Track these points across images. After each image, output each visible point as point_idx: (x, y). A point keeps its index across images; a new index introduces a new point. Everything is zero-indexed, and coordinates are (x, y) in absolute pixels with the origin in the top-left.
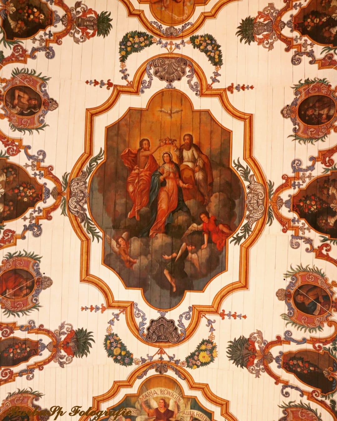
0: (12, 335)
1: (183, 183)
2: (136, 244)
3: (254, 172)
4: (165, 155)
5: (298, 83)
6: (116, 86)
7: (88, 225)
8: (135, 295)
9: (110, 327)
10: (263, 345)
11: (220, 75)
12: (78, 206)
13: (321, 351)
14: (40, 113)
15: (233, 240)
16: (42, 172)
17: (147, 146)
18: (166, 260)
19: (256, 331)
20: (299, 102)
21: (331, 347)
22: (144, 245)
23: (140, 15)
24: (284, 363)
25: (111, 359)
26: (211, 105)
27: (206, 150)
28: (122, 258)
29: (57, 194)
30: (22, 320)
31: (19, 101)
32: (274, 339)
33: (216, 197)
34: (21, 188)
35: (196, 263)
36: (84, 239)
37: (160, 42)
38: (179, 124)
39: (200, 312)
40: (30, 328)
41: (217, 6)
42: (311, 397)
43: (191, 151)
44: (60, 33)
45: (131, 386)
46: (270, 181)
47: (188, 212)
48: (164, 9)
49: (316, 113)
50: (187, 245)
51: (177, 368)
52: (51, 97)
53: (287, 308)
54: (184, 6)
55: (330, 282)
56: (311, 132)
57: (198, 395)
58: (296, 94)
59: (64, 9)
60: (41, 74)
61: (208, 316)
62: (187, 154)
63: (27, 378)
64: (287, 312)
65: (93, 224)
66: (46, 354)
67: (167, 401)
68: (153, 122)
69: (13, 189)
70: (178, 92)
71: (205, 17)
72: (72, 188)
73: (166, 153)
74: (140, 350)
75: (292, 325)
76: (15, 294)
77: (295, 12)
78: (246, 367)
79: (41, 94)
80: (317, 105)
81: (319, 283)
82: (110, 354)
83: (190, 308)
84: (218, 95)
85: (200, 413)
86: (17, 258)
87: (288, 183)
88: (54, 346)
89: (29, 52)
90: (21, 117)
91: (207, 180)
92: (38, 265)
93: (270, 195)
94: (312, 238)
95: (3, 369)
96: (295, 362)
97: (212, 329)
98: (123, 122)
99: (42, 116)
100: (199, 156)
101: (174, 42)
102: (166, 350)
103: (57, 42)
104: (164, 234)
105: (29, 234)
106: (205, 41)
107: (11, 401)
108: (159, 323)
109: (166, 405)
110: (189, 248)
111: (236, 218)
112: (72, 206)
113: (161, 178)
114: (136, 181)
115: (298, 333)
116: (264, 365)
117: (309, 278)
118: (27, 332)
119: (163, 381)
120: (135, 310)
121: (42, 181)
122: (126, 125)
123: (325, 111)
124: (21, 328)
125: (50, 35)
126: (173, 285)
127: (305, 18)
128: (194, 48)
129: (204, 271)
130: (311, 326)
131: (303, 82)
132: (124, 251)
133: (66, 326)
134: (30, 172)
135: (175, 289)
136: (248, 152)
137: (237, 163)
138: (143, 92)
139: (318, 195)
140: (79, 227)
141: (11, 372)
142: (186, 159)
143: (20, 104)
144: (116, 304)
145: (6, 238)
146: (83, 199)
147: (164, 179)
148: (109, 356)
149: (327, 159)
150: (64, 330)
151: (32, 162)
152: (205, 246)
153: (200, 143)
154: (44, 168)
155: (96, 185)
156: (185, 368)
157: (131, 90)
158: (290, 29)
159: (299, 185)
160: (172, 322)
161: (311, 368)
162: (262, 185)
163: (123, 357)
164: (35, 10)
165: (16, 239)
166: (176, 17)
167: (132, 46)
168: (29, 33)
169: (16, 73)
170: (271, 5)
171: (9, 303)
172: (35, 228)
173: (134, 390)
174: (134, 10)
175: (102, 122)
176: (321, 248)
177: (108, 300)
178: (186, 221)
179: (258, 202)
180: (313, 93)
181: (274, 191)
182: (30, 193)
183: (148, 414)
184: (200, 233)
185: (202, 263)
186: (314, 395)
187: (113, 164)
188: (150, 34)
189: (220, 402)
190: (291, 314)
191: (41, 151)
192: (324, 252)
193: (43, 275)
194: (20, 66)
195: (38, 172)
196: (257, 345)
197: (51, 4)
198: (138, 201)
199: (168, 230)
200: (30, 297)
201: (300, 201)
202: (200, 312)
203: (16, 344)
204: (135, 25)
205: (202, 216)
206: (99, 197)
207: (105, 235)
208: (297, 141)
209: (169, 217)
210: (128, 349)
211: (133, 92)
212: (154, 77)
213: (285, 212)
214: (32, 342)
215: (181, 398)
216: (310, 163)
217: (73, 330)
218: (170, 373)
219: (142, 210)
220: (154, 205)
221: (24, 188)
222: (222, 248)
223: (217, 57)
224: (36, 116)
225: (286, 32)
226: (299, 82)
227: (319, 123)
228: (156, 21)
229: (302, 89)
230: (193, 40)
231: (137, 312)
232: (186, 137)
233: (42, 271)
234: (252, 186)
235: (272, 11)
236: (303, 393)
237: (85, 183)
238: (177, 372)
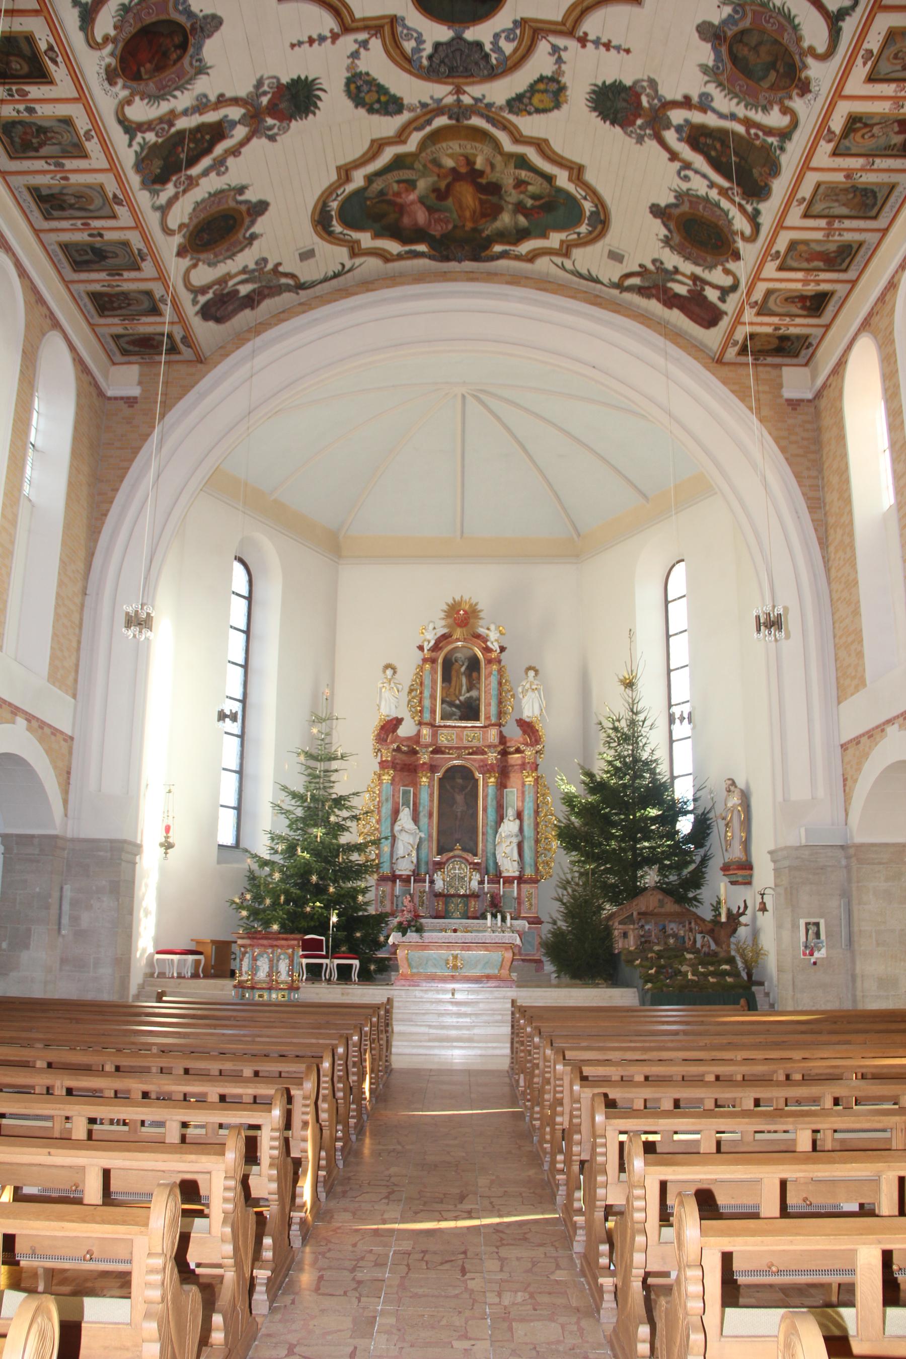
0: (173, 130)
9: (353, 62)
10: (656, 101)
19: (646, 78)
21: (776, 143)
25: (362, 112)
30: (183, 100)
32: (679, 97)
42: (723, 192)
45: (404, 142)
51: (491, 114)
53: (712, 57)
55: (805, 44)
61: (552, 39)
64: (711, 63)
66: (240, 132)
75: (716, 87)
78: (622, 127)
81: (786, 38)
83: (515, 22)
85: (532, 175)
86: (139, 7)
97: (559, 61)
102: (467, 89)
115: (722, 102)
116: (653, 129)
117: (768, 22)
120: (400, 29)
124: (185, 113)
130: (751, 101)
133: (267, 82)
141: (190, 178)
144: (360, 24)
148: (356, 107)
150: (266, 88)
160: (479, 45)
163: (385, 103)
177: (342, 19)
186: (730, 192)
189: (569, 164)
190: (718, 68)
193: (201, 15)
210: (393, 91)
215: (497, 154)
217: (283, 85)
218: (476, 121)
231: (405, 31)
233: (195, 8)
236: (712, 185)
238: (489, 120)
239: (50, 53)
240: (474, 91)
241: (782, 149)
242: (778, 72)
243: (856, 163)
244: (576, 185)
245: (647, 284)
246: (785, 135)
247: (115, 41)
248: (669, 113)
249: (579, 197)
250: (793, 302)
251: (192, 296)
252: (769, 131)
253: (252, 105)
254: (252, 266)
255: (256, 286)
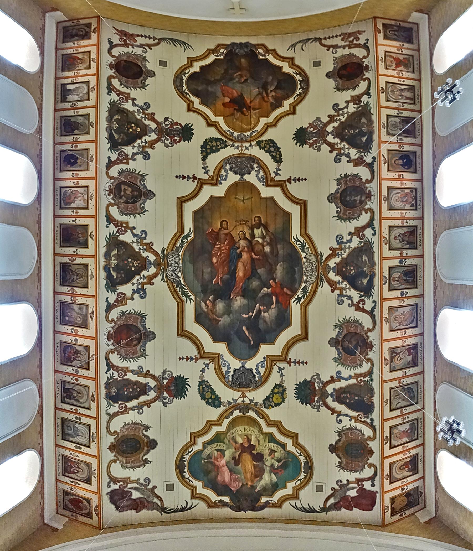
0: (125, 377)
1: (255, 255)
2: (220, 306)
3: (309, 245)
4: (241, 233)
5: (339, 177)
6: (199, 179)
7: (182, 290)
8: (221, 348)
9: (202, 374)
10: (321, 385)
11: (281, 170)
12: (174, 275)
13: (362, 384)
14: (141, 201)
15: (295, 301)
16: (145, 247)
17: (226, 226)
18: (244, 318)
20: (340, 191)
22: (227, 306)
23: (216, 125)
24: (336, 397)
25: (204, 402)
26: (274, 193)
27: (271, 229)
28: (210, 317)
29: (157, 264)
30: (133, 365)
31: (125, 192)
32: (329, 379)
33: (281, 265)
34: (130, 260)
35: (267, 320)
36: (179, 301)
37: (233, 146)
38: (250, 207)
39: (272, 361)
40: (139, 372)
41: (277, 119)
42: (357, 420)
43: (260, 229)
44: (153, 140)
46: (321, 252)
47: (260, 278)
48: (235, 120)
49: (352, 199)
50: (260, 305)
52: (149, 189)
54: (251, 118)
56: (349, 213)
57: (274, 430)
58: (338, 185)
59: (155, 123)
60: (140, 172)
62: (257, 232)
63: (138, 413)
64: (337, 356)
65: (186, 289)
66: (152, 394)
67: (249, 437)
68: (230, 207)
69: (123, 261)
70: (249, 183)
71: (268, 127)
72: (168, 260)
73: (241, 231)
74: (227, 394)
76: (127, 344)
77: (336, 124)
79: (142, 187)
80: (353, 193)
82: (203, 397)
84: (280, 185)
87: (334, 253)
88: (158, 389)
89: (130, 156)
90: (126, 204)
91: (273, 252)
92: (144, 322)
93: (321, 263)
94: (352, 296)
95: (119, 403)
96: (345, 395)
97: (282, 375)
98: (206, 207)
99: (142, 203)
100: (266, 234)
101: (244, 145)
103: (151, 148)
104: (242, 297)
105: (136, 296)
106: (268, 144)
107: (126, 429)
108: (240, 371)
109: (249, 440)
110: (262, 308)
111: (296, 282)
112: (169, 275)
113: (238, 251)
114: (219, 254)
115: (346, 372)
116: (322, 401)
118: (137, 375)
119: (246, 420)
120: (221, 360)
121: (145, 254)
122: (209, 209)
123: (358, 198)
124: (133, 371)
125: (146, 142)
126: (251, 339)
127: (343, 129)
128: (260, 149)
129: (274, 326)
130: (354, 365)
131: (343, 176)
132: (211, 311)
133: (167, 373)
134: (136, 247)
135: (252, 343)
136: (303, 230)
137: (296, 239)
138: (221, 183)
139: (355, 262)
140: (176, 291)
141: (126, 406)
142: (256, 236)
143: (126, 195)
145: (119, 299)
146: (177, 269)
147: (241, 252)
149: (361, 234)
150: (166, 376)
151: (137, 240)
152: (274, 306)
153: (267, 223)
154: (146, 244)
155: (187, 258)
156: (262, 409)
157: (212, 182)
158: (333, 137)
159: (342, 254)
160: (251, 370)
161: (356, 398)
162: (315, 256)
163: (214, 401)
164: (133, 125)
165: (127, 300)
166: (245, 127)
167: (211, 148)
168: (130, 141)
169: (121, 172)
170: (319, 119)
171: (123, 351)
172: (141, 292)
173: (223, 428)
174: (211, 121)
175: (191, 207)
176: (358, 303)
178: (259, 286)
179: (312, 269)
180: (349, 184)
181: (324, 260)
182: (136, 263)
183: (235, 448)
184: (269, 295)
185: (272, 320)
186: (359, 417)
187: (200, 240)
188: (225, 139)
190: (340, 357)
191: (143, 231)
192: (361, 306)
193: (149, 330)
194: (124, 167)
195: (141, 247)
196: (316, 385)
197: (145, 120)
198: (220, 270)
199: (245, 293)
200: (139, 347)
201: (343, 267)
202: (272, 361)
203: (129, 384)
204: (213, 133)
205: (270, 282)
206: (190, 267)
207: (196, 298)
208: (339, 220)
209: (244, 283)
211: (213, 184)
212: (229, 172)
213: (332, 276)
214: (141, 383)
215: (260, 434)
216: (349, 237)
218: (251, 414)
219: (224, 277)
220: (233, 273)
221: (132, 260)
222: (287, 308)
223: (278, 156)
224: (138, 204)
225: (330, 138)
226: (340, 176)
227: (354, 207)
228: (229, 129)
229: (342, 181)
230: (259, 144)
231: (223, 362)
232: (256, 219)
234: (308, 256)
235: (319, 123)
236: (351, 418)
237: (179, 256)
238: (257, 413)
239: (92, 314)
240: (251, 395)
241: (372, 380)
242: (360, 346)
243: (399, 374)
244: (296, 447)
245: (337, 501)
246: (370, 372)
247: (115, 323)
248: (326, 389)
249: (298, 455)
250: (404, 469)
251: (108, 480)
252: (365, 375)
253: (160, 382)
254: (142, 481)
255: (142, 496)
